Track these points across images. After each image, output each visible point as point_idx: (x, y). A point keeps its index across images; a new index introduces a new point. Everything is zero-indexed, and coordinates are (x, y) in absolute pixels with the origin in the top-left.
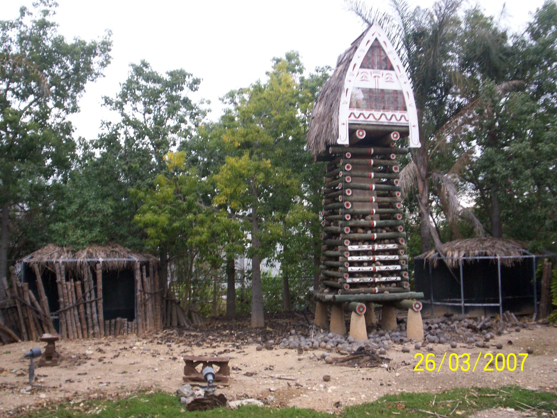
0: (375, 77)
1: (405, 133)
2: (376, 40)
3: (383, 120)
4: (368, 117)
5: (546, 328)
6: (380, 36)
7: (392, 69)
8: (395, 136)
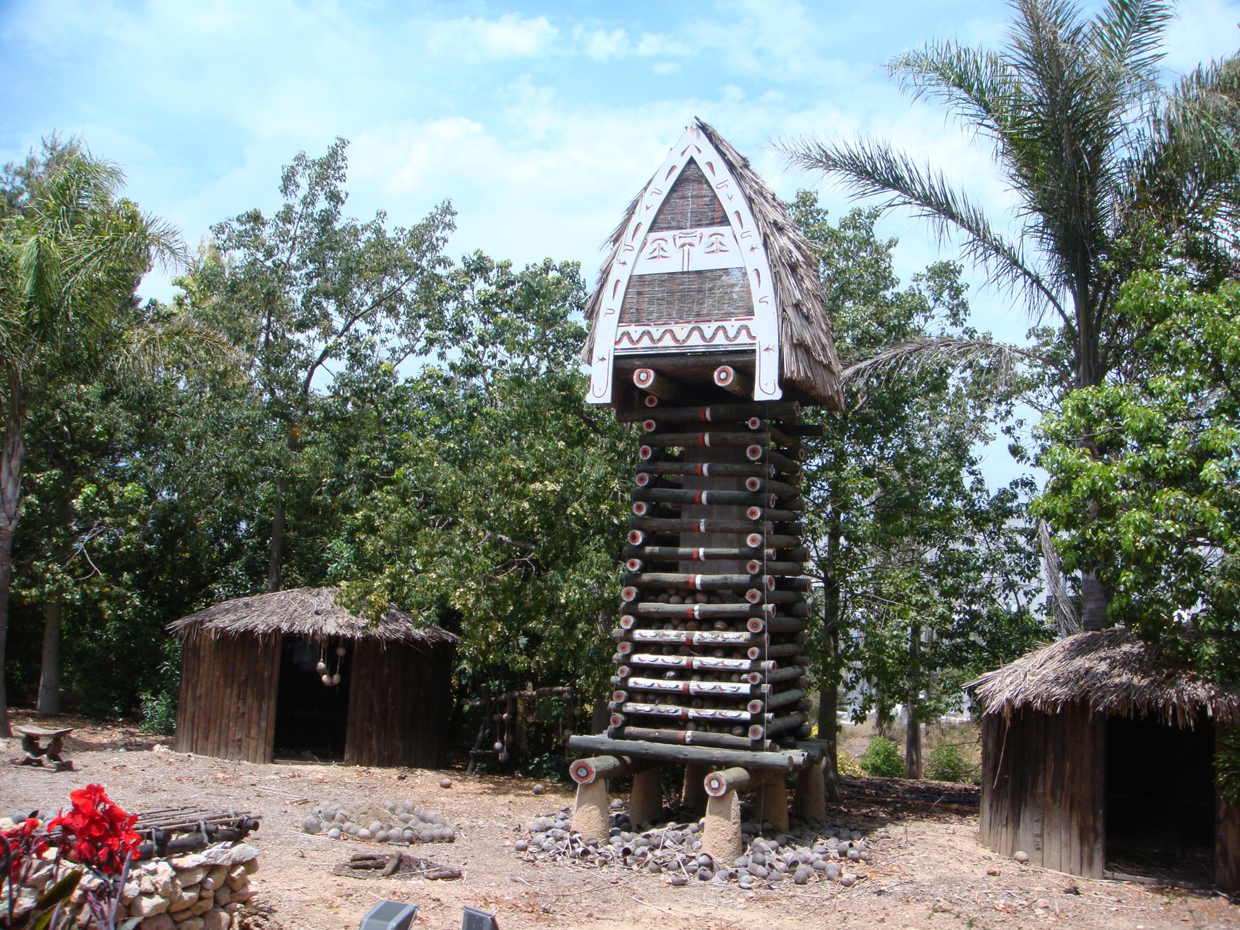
0: (683, 246)
1: (746, 373)
2: (692, 161)
3: (695, 341)
4: (640, 338)
5: (1194, 902)
6: (700, 151)
7: (724, 221)
8: (723, 375)
